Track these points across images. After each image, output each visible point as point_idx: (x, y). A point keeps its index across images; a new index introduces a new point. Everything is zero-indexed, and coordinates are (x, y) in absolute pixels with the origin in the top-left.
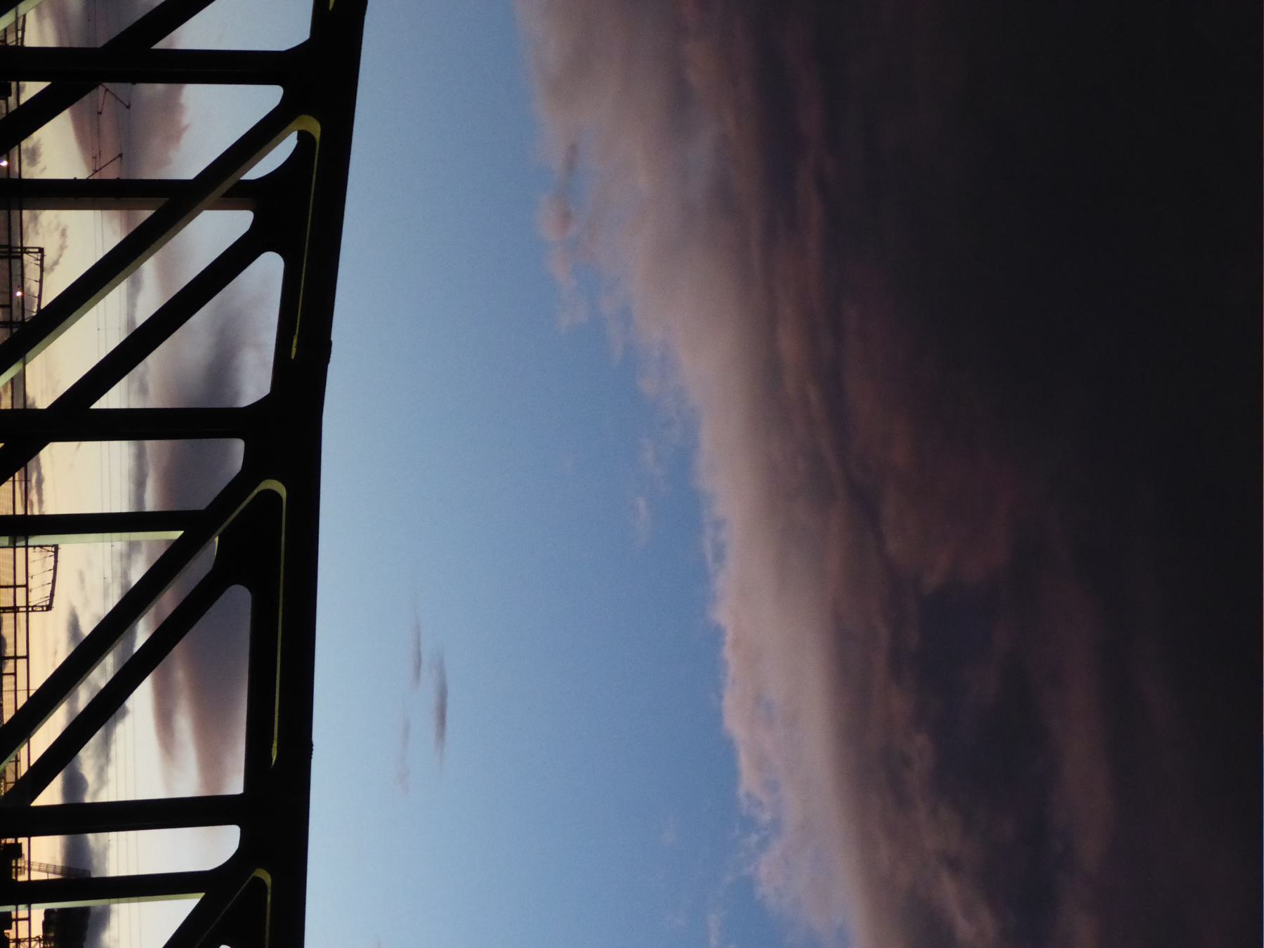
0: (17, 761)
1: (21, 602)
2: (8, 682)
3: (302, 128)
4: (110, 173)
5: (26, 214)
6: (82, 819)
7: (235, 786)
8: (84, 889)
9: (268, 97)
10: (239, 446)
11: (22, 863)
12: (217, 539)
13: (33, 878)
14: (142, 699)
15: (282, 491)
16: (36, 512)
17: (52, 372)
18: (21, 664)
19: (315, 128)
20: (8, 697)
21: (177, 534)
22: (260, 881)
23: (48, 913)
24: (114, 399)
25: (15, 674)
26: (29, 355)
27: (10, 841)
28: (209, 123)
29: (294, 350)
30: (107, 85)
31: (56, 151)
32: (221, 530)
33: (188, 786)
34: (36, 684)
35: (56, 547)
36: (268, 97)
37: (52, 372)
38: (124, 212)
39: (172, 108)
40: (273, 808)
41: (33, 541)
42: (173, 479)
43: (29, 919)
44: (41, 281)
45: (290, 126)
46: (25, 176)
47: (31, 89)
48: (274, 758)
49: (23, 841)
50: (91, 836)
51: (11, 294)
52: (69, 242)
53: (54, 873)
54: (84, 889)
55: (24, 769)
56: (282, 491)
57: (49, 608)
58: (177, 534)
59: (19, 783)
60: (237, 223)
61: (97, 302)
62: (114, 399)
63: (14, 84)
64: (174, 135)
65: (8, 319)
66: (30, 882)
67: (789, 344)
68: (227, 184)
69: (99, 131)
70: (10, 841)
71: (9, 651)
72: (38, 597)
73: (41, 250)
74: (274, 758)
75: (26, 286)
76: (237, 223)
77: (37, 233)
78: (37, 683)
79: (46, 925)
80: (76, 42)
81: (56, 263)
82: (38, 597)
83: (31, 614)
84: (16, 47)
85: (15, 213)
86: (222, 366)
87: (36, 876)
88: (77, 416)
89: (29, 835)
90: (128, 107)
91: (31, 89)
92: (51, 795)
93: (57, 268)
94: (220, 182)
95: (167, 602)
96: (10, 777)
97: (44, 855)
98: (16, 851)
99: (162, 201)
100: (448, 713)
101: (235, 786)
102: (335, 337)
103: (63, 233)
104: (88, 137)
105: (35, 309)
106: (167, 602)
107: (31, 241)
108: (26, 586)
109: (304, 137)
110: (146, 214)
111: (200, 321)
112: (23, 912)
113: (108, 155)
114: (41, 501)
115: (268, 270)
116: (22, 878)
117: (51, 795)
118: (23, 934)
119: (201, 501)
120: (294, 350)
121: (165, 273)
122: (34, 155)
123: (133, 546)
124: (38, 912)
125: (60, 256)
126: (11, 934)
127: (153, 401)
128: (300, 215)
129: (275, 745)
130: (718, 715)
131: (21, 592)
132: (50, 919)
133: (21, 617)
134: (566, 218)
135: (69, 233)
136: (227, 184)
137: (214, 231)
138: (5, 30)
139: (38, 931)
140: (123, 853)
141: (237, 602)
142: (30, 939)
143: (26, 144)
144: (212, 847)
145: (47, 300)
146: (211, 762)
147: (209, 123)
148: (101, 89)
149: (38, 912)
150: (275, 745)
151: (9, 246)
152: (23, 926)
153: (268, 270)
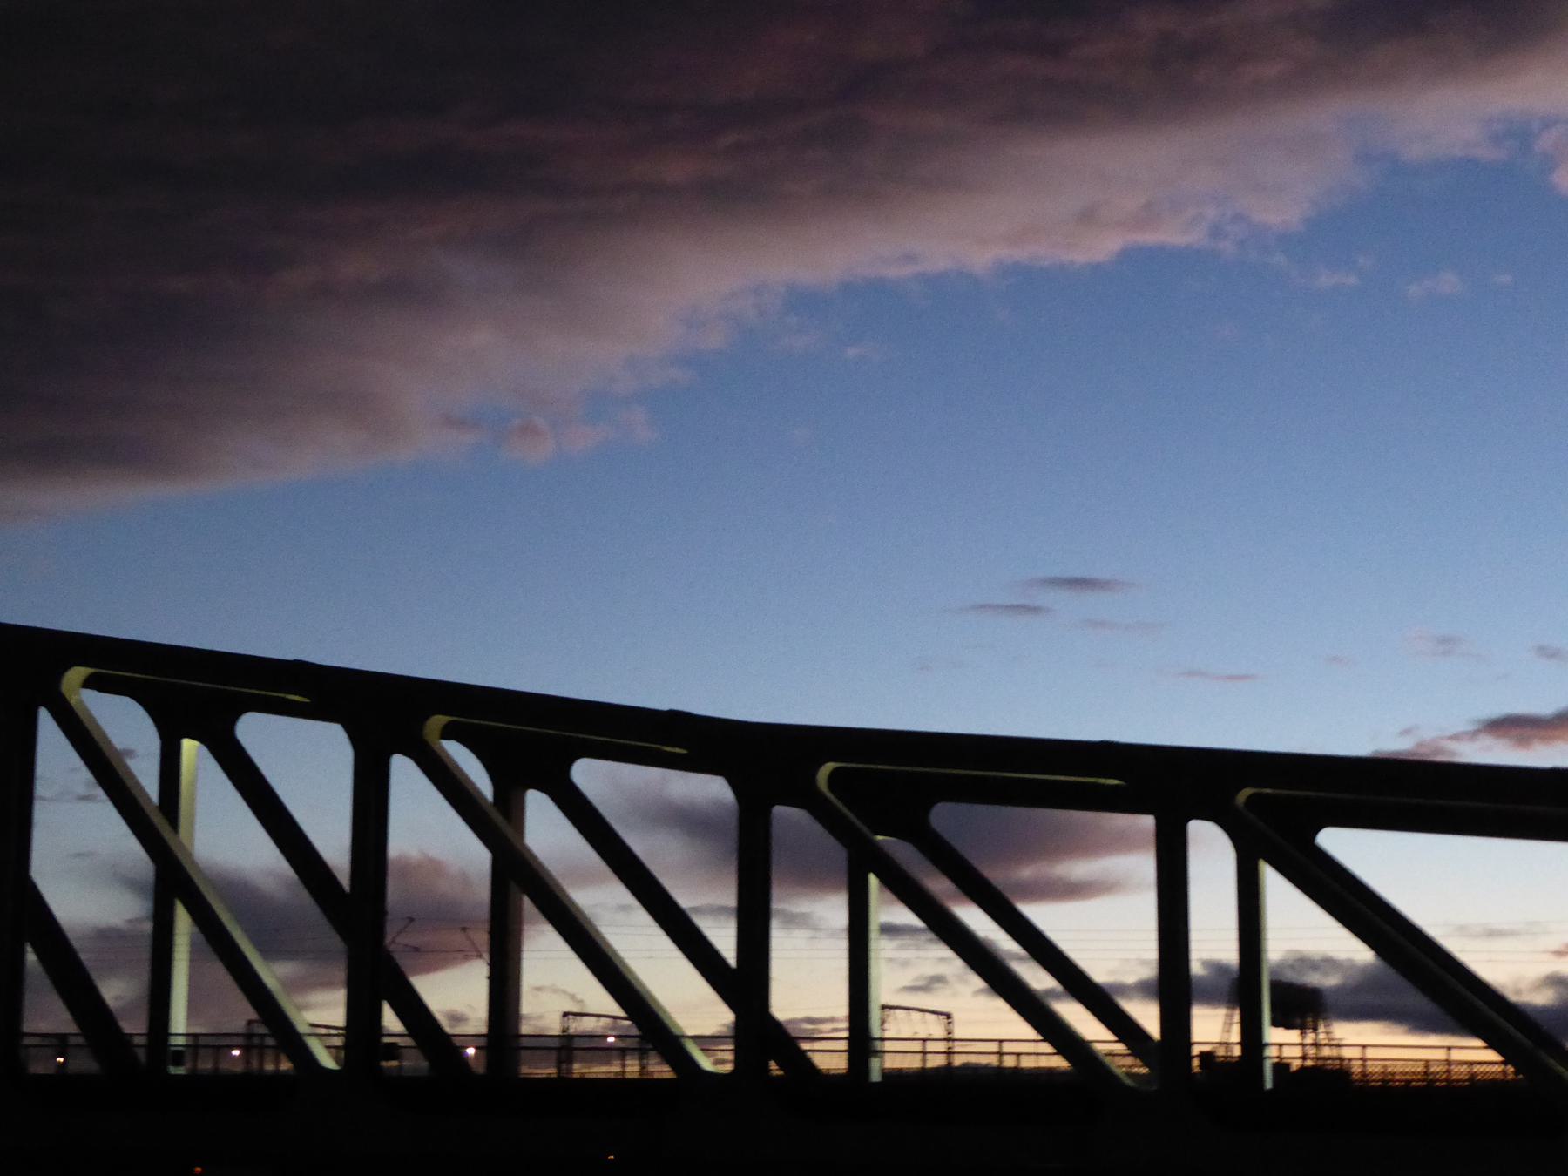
0: (1111, 1054)
1: (942, 1047)
2: (1027, 1063)
3: (437, 733)
4: (482, 938)
5: (525, 1029)
6: (1174, 983)
7: (1148, 822)
8: (1245, 985)
9: (403, 770)
10: (779, 811)
11: (1221, 1052)
12: (880, 838)
13: (929, 1065)
14: (1038, 914)
15: (829, 767)
16: (845, 1025)
17: (696, 1009)
18: (1007, 1048)
19: (438, 721)
20: (1045, 1062)
21: (873, 881)
22: (1250, 798)
23: (1276, 1023)
24: (724, 939)
25: (1019, 1054)
26: (677, 1032)
27: (1196, 1063)
28: (429, 832)
29: (677, 750)
30: (388, 939)
31: (456, 994)
32: (865, 829)
33: (1143, 866)
34: (1031, 1033)
35: (884, 1007)
36: (403, 770)
37: (696, 1009)
38: (526, 927)
39: (407, 868)
40: (1170, 787)
41: (876, 1033)
42: (812, 879)
43: (1281, 1045)
44: (599, 1016)
45: (436, 748)
46: (483, 1030)
47: (391, 1021)
48: (1115, 782)
49: (1196, 1050)
51: (610, 1048)
52: (556, 990)
53: (1231, 1016)
54: (1245, 985)
55: (1120, 1047)
56: (829, 767)
57: (948, 1016)
58: (873, 881)
59: (1135, 1052)
61: (622, 961)
62: (724, 939)
63: (387, 1040)
64: (434, 868)
65: (554, 1054)
66: (1242, 1044)
67: (677, 169)
69: (417, 949)
70: (1196, 1063)
71: (993, 1061)
72: (936, 1028)
73: (566, 1015)
74: (1115, 782)
75: (599, 1032)
77: (541, 1017)
78: (1028, 1032)
79: (1288, 1026)
80: (341, 974)
81: (573, 997)
82: (936, 1028)
83: (956, 1036)
84: (347, 1036)
85: (525, 1042)
86: (689, 821)
87: (1235, 1036)
88: (743, 983)
89: (1189, 1044)
90: (411, 920)
91: (391, 1021)
92: (1148, 1016)
93: (579, 997)
94: (495, 824)
95: (938, 885)
96: (1129, 1061)
97: (1212, 1028)
98: (1206, 1057)
99: (514, 888)
100: (1078, 574)
101: (1148, 822)
102: (664, 705)
103: (539, 989)
104: (439, 958)
105: (628, 1023)
106: (938, 885)
107: (554, 1026)
108: (924, 1040)
109: (447, 733)
110: (527, 902)
111: (639, 843)
112: (1271, 1052)
113: (458, 938)
114: (832, 1020)
115: (588, 774)
116: (1237, 1051)
117: (1148, 1016)
118: (1297, 1052)
119: (837, 853)
120: (677, 750)
121: (587, 879)
122: (457, 1018)
123: (889, 930)
124: (1274, 1035)
125: (564, 992)
126: (1296, 1064)
127: (728, 897)
128: (533, 740)
129: (1102, 781)
130: (1096, 268)
131: (930, 1046)
132: (1279, 1021)
133: (958, 1047)
134: (528, 430)
135: (539, 984)
137: (546, 830)
138: (328, 1047)
139: (1293, 1036)
140: (1213, 940)
141: (945, 817)
142: (1303, 1045)
143: (448, 1028)
144: (1211, 853)
145: (614, 1009)
146: (1120, 843)
147: (429, 832)
148: (392, 948)
149: (1274, 1035)
150: (1102, 781)
151: (559, 1049)
152: (1288, 1052)
153: (588, 774)
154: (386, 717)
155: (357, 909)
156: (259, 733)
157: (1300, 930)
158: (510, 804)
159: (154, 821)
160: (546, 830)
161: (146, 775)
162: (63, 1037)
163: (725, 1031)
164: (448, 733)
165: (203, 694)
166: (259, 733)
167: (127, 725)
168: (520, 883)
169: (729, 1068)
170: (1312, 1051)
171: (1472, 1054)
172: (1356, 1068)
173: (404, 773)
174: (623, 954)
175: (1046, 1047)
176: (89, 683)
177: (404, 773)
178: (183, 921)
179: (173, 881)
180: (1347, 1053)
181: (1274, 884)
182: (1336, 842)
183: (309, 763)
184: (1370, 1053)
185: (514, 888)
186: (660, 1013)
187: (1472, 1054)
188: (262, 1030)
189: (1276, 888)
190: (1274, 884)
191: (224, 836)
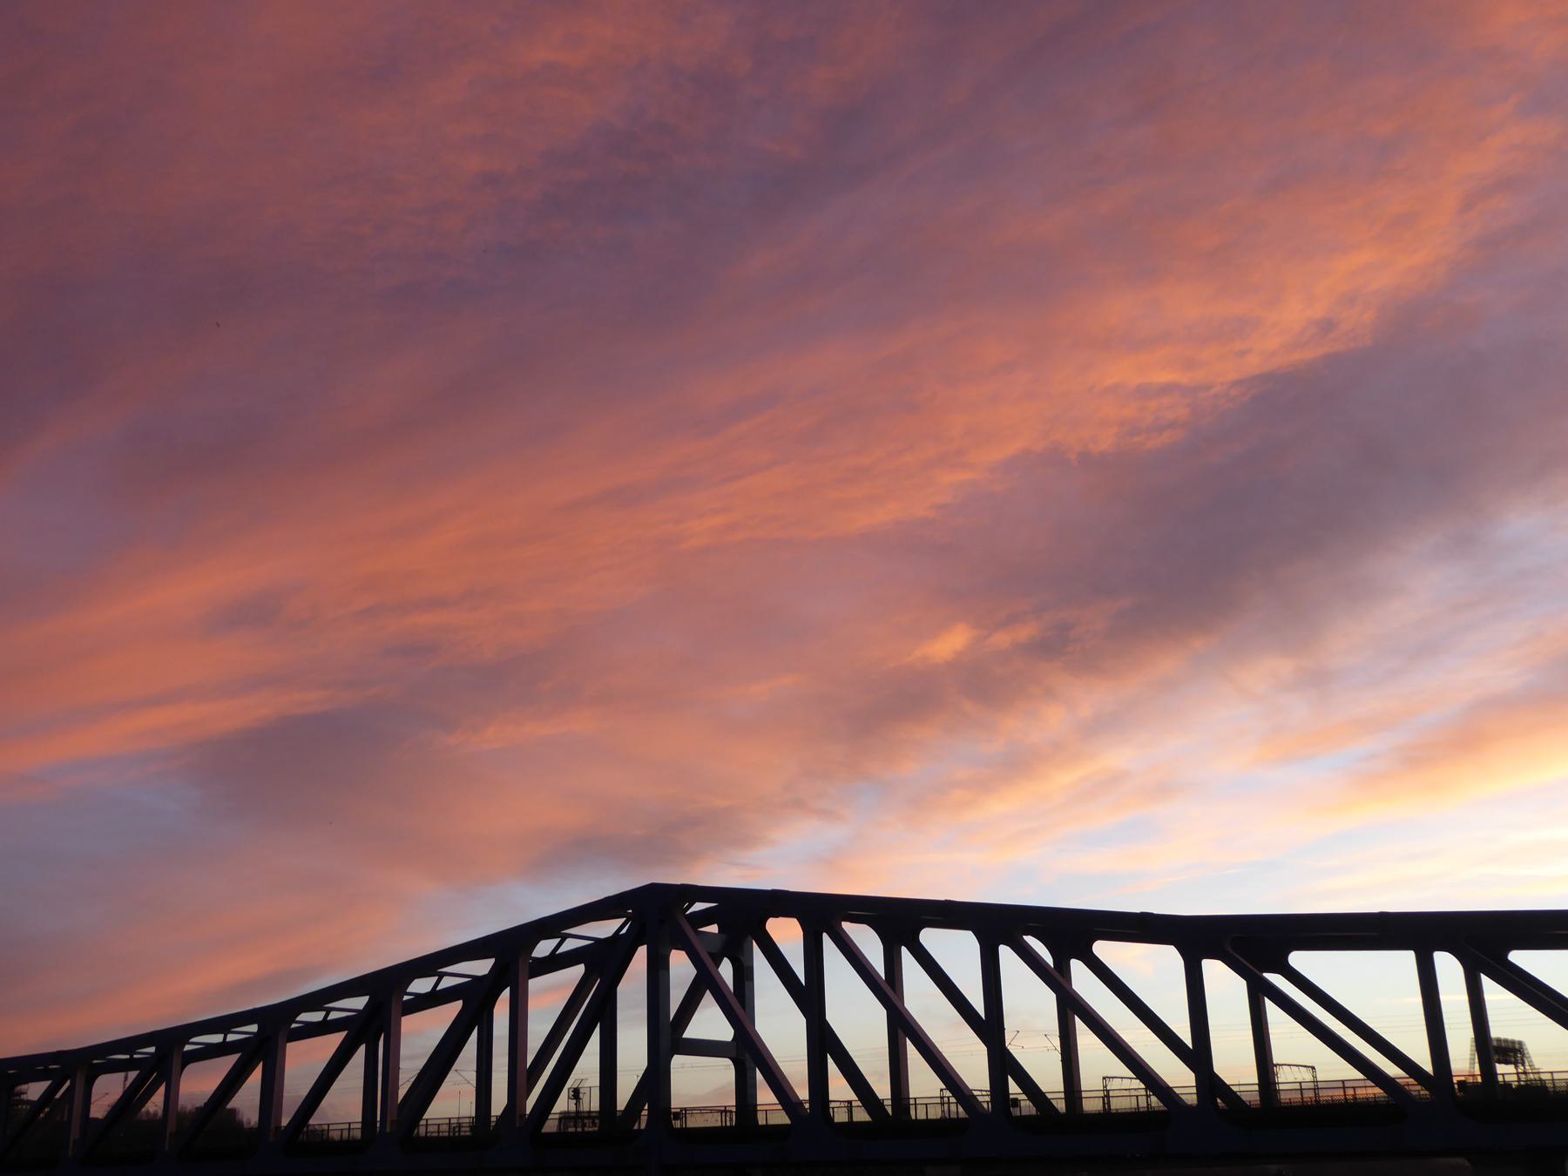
9: (1006, 954)
11: (1471, 1080)
17: (1178, 1075)
37: (1178, 1075)
47: (1014, 1088)
49: (1455, 1080)
50: (311, 1122)
55: (1411, 1081)
60: (1077, 968)
68: (1057, 975)
72: (1307, 1076)
76: (1077, 968)
79: (1507, 1063)
85: (1281, 1087)
87: (1477, 1070)
89: (1451, 1076)
91: (1014, 1088)
99: (900, 1032)
102: (1138, 911)
110: (1077, 1019)
124: (1501, 1068)
126: (1515, 1085)
136: (1057, 975)
137: (1082, 978)
144: (1448, 967)
149: (1501, 1068)
152: (1508, 1078)
153: (1101, 949)
156: (931, 938)
157: (1509, 1015)
162: (850, 1102)
163: (191, 1068)
166: (931, 938)
169: (761, 1121)
170: (1523, 1077)
172: (1549, 1085)
175: (1369, 1083)
180: (1544, 1077)
181: (1487, 983)
182: (1518, 957)
184: (1556, 1076)
188: (948, 1093)
189: (1493, 992)
190: (1487, 983)
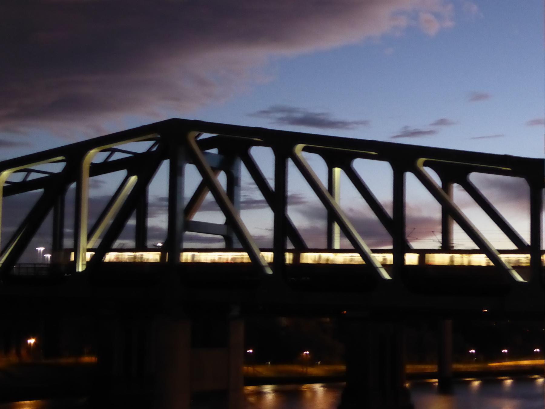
3: (422, 164)
19: (421, 160)
94: (441, 196)
99: (450, 218)
128: (455, 166)
137: (459, 195)
153: (474, 177)
154: (402, 158)
155: (395, 224)
158: (446, 187)
159: (326, 195)
160: (459, 195)
161: (324, 182)
164: (425, 164)
165: (342, 153)
166: (360, 165)
167: (317, 164)
168: (451, 214)
171: (47, 175)
173: (410, 178)
174: (489, 240)
176: (304, 149)
177: (410, 178)
178: (337, 229)
179: (333, 216)
183: (378, 175)
185: (450, 218)
186: (478, 232)
187: (47, 175)
191: (347, 199)
